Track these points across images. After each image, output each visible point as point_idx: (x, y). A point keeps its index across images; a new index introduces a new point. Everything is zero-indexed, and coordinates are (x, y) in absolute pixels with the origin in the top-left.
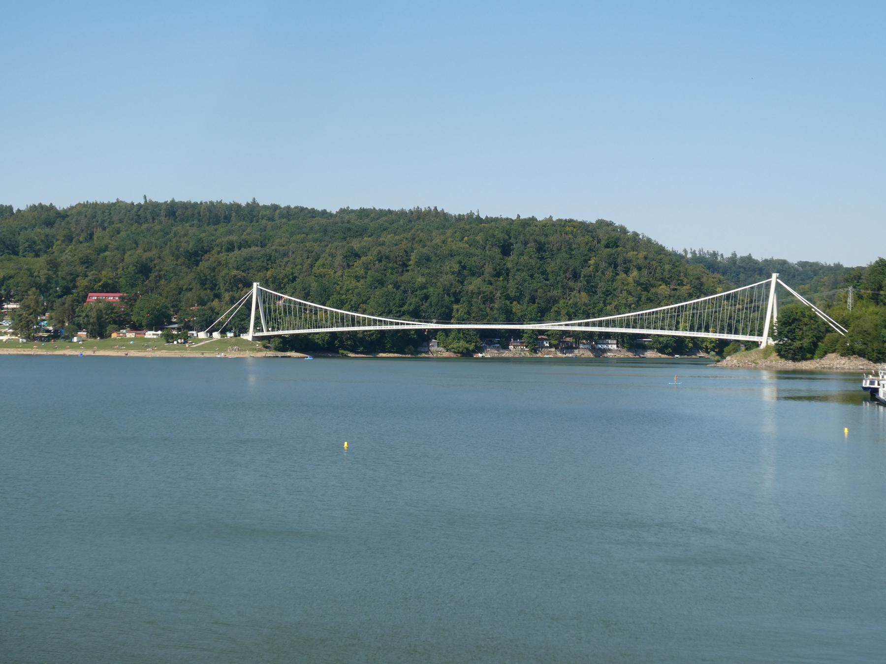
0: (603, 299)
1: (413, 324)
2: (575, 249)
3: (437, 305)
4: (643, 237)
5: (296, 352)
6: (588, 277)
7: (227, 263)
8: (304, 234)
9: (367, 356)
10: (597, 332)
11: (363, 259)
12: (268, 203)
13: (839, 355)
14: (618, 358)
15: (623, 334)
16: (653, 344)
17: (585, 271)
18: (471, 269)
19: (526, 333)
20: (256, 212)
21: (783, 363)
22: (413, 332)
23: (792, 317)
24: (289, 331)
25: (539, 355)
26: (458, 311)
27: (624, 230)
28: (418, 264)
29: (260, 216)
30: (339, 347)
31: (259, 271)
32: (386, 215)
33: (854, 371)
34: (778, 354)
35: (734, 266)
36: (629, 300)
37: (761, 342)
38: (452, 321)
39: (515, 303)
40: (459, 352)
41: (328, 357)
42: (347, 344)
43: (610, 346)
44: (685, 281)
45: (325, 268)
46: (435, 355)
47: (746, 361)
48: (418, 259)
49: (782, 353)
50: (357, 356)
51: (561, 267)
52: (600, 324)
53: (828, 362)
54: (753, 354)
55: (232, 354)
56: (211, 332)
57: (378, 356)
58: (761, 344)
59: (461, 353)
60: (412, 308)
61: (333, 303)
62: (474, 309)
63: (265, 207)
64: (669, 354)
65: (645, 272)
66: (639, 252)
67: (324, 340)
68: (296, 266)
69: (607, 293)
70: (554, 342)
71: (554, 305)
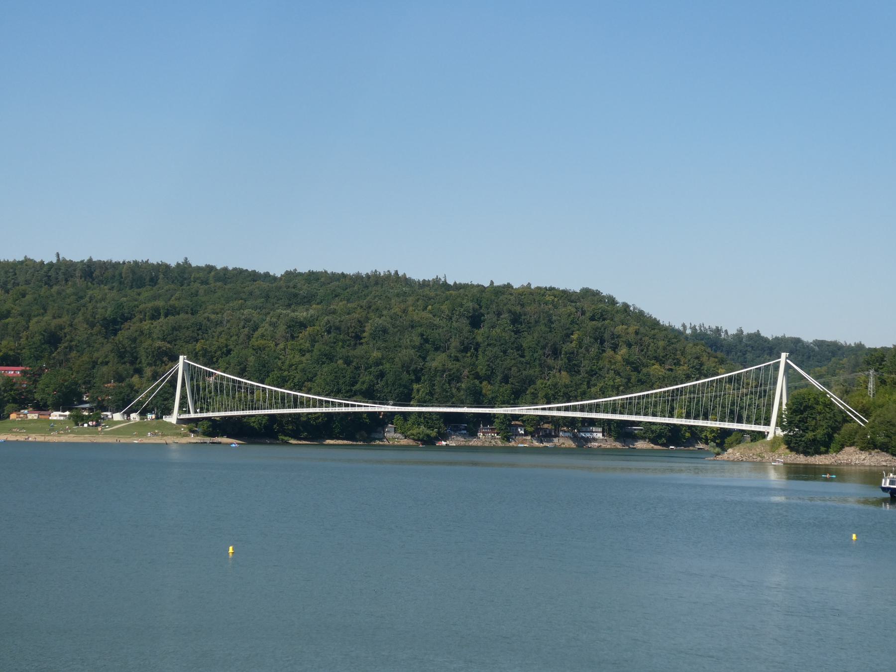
0: (586, 380)
1: (365, 406)
3: (393, 384)
4: (634, 308)
5: (228, 437)
6: (570, 354)
7: (150, 333)
8: (241, 299)
9: (312, 443)
10: (579, 418)
12: (202, 264)
13: (858, 449)
14: (606, 450)
15: (609, 421)
16: (644, 434)
19: (498, 418)
22: (365, 415)
23: (804, 405)
25: (512, 444)
26: (418, 391)
27: (612, 301)
28: (374, 336)
29: (192, 279)
31: (188, 342)
34: (786, 446)
36: (616, 381)
37: (768, 433)
38: (412, 403)
39: (485, 383)
40: (418, 440)
41: (266, 444)
44: (682, 360)
47: (751, 455)
49: (792, 445)
51: (539, 342)
52: (582, 409)
53: (846, 457)
54: (759, 446)
55: (150, 439)
56: (128, 413)
58: (767, 435)
60: (365, 387)
61: (273, 381)
64: (663, 445)
66: (629, 326)
67: (260, 424)
68: (231, 337)
69: (592, 373)
70: (530, 429)
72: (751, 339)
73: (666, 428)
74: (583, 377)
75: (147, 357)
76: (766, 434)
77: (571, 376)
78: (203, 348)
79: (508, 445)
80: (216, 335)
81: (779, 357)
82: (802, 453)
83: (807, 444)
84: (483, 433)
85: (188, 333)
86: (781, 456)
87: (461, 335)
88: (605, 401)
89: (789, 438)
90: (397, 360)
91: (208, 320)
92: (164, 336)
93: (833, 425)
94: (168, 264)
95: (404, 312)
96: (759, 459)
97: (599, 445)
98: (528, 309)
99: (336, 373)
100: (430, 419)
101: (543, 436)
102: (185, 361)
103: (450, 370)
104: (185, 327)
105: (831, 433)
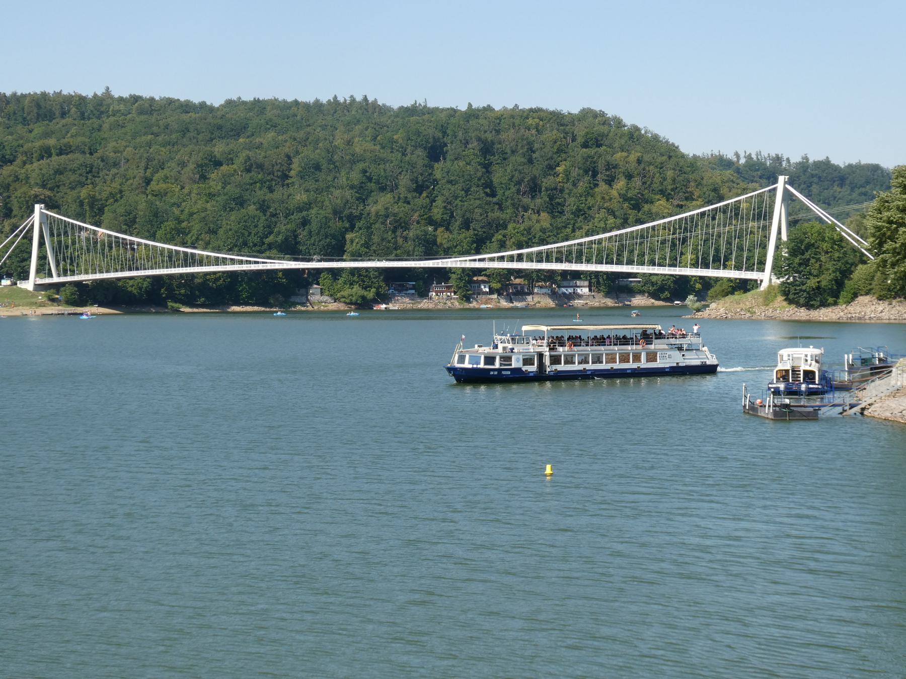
0: (572, 222)
2: (537, 149)
3: (318, 233)
4: (646, 133)
5: (101, 305)
7: (27, 178)
8: (152, 134)
9: (212, 311)
10: (559, 270)
11: (224, 168)
14: (593, 308)
15: (597, 274)
16: (642, 287)
17: (547, 182)
18: (378, 180)
20: (105, 107)
21: (791, 312)
23: (806, 242)
24: (124, 273)
25: (474, 305)
26: (352, 241)
27: (619, 123)
28: (302, 176)
30: (168, 297)
31: (72, 188)
32: (446, 110)
33: (897, 322)
34: (784, 298)
35: (804, 174)
36: (609, 222)
37: (761, 281)
38: (344, 257)
39: (440, 230)
40: (351, 303)
42: (180, 294)
43: (579, 291)
45: (168, 182)
46: (316, 308)
47: (738, 310)
48: (302, 167)
49: (791, 296)
50: (195, 310)
51: (513, 176)
52: (539, 258)
53: (858, 309)
54: (747, 300)
57: (229, 310)
58: (761, 284)
59: (355, 304)
61: (165, 234)
62: (376, 239)
63: (121, 99)
64: (665, 300)
65: (637, 182)
66: (630, 153)
67: (140, 289)
68: (127, 180)
69: (578, 212)
70: (496, 286)
71: (497, 232)
72: (819, 168)
73: (669, 279)
74: (568, 219)
75: (21, 208)
76: (759, 282)
77: (554, 217)
78: (90, 195)
79: (468, 307)
80: (109, 178)
81: (775, 181)
82: (803, 306)
83: (809, 294)
84: (437, 292)
85: (73, 177)
86: (776, 310)
87: (414, 170)
88: (557, 248)
89: (786, 287)
90: (327, 203)
91: (103, 161)
92: (44, 181)
93: (843, 268)
94: (84, 95)
95: (348, 144)
96: (748, 315)
97: (585, 302)
98: (503, 136)
99: (245, 222)
100: (366, 276)
101: (514, 294)
102: (42, 210)
103: (395, 215)
104: (70, 170)
105: (839, 278)
